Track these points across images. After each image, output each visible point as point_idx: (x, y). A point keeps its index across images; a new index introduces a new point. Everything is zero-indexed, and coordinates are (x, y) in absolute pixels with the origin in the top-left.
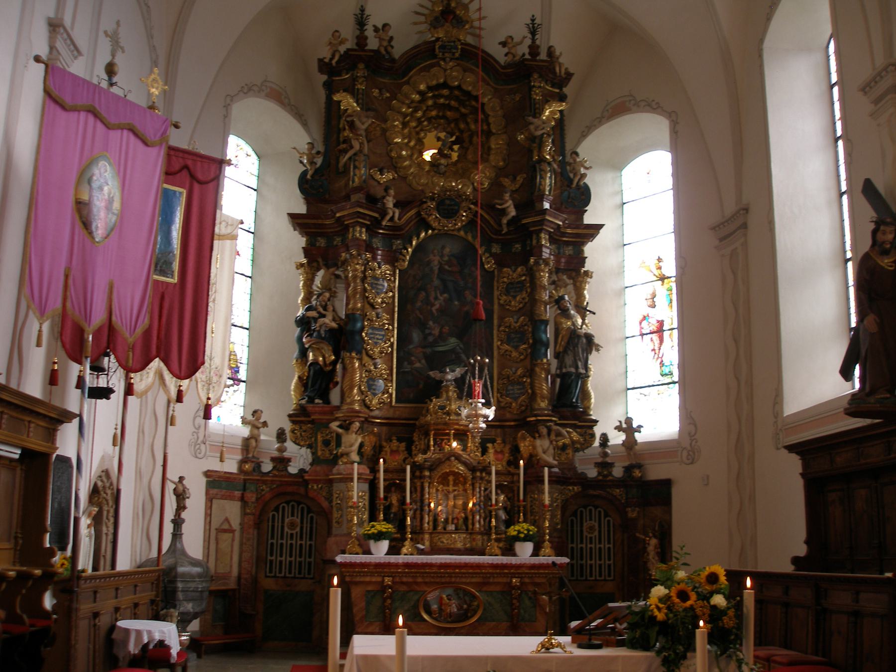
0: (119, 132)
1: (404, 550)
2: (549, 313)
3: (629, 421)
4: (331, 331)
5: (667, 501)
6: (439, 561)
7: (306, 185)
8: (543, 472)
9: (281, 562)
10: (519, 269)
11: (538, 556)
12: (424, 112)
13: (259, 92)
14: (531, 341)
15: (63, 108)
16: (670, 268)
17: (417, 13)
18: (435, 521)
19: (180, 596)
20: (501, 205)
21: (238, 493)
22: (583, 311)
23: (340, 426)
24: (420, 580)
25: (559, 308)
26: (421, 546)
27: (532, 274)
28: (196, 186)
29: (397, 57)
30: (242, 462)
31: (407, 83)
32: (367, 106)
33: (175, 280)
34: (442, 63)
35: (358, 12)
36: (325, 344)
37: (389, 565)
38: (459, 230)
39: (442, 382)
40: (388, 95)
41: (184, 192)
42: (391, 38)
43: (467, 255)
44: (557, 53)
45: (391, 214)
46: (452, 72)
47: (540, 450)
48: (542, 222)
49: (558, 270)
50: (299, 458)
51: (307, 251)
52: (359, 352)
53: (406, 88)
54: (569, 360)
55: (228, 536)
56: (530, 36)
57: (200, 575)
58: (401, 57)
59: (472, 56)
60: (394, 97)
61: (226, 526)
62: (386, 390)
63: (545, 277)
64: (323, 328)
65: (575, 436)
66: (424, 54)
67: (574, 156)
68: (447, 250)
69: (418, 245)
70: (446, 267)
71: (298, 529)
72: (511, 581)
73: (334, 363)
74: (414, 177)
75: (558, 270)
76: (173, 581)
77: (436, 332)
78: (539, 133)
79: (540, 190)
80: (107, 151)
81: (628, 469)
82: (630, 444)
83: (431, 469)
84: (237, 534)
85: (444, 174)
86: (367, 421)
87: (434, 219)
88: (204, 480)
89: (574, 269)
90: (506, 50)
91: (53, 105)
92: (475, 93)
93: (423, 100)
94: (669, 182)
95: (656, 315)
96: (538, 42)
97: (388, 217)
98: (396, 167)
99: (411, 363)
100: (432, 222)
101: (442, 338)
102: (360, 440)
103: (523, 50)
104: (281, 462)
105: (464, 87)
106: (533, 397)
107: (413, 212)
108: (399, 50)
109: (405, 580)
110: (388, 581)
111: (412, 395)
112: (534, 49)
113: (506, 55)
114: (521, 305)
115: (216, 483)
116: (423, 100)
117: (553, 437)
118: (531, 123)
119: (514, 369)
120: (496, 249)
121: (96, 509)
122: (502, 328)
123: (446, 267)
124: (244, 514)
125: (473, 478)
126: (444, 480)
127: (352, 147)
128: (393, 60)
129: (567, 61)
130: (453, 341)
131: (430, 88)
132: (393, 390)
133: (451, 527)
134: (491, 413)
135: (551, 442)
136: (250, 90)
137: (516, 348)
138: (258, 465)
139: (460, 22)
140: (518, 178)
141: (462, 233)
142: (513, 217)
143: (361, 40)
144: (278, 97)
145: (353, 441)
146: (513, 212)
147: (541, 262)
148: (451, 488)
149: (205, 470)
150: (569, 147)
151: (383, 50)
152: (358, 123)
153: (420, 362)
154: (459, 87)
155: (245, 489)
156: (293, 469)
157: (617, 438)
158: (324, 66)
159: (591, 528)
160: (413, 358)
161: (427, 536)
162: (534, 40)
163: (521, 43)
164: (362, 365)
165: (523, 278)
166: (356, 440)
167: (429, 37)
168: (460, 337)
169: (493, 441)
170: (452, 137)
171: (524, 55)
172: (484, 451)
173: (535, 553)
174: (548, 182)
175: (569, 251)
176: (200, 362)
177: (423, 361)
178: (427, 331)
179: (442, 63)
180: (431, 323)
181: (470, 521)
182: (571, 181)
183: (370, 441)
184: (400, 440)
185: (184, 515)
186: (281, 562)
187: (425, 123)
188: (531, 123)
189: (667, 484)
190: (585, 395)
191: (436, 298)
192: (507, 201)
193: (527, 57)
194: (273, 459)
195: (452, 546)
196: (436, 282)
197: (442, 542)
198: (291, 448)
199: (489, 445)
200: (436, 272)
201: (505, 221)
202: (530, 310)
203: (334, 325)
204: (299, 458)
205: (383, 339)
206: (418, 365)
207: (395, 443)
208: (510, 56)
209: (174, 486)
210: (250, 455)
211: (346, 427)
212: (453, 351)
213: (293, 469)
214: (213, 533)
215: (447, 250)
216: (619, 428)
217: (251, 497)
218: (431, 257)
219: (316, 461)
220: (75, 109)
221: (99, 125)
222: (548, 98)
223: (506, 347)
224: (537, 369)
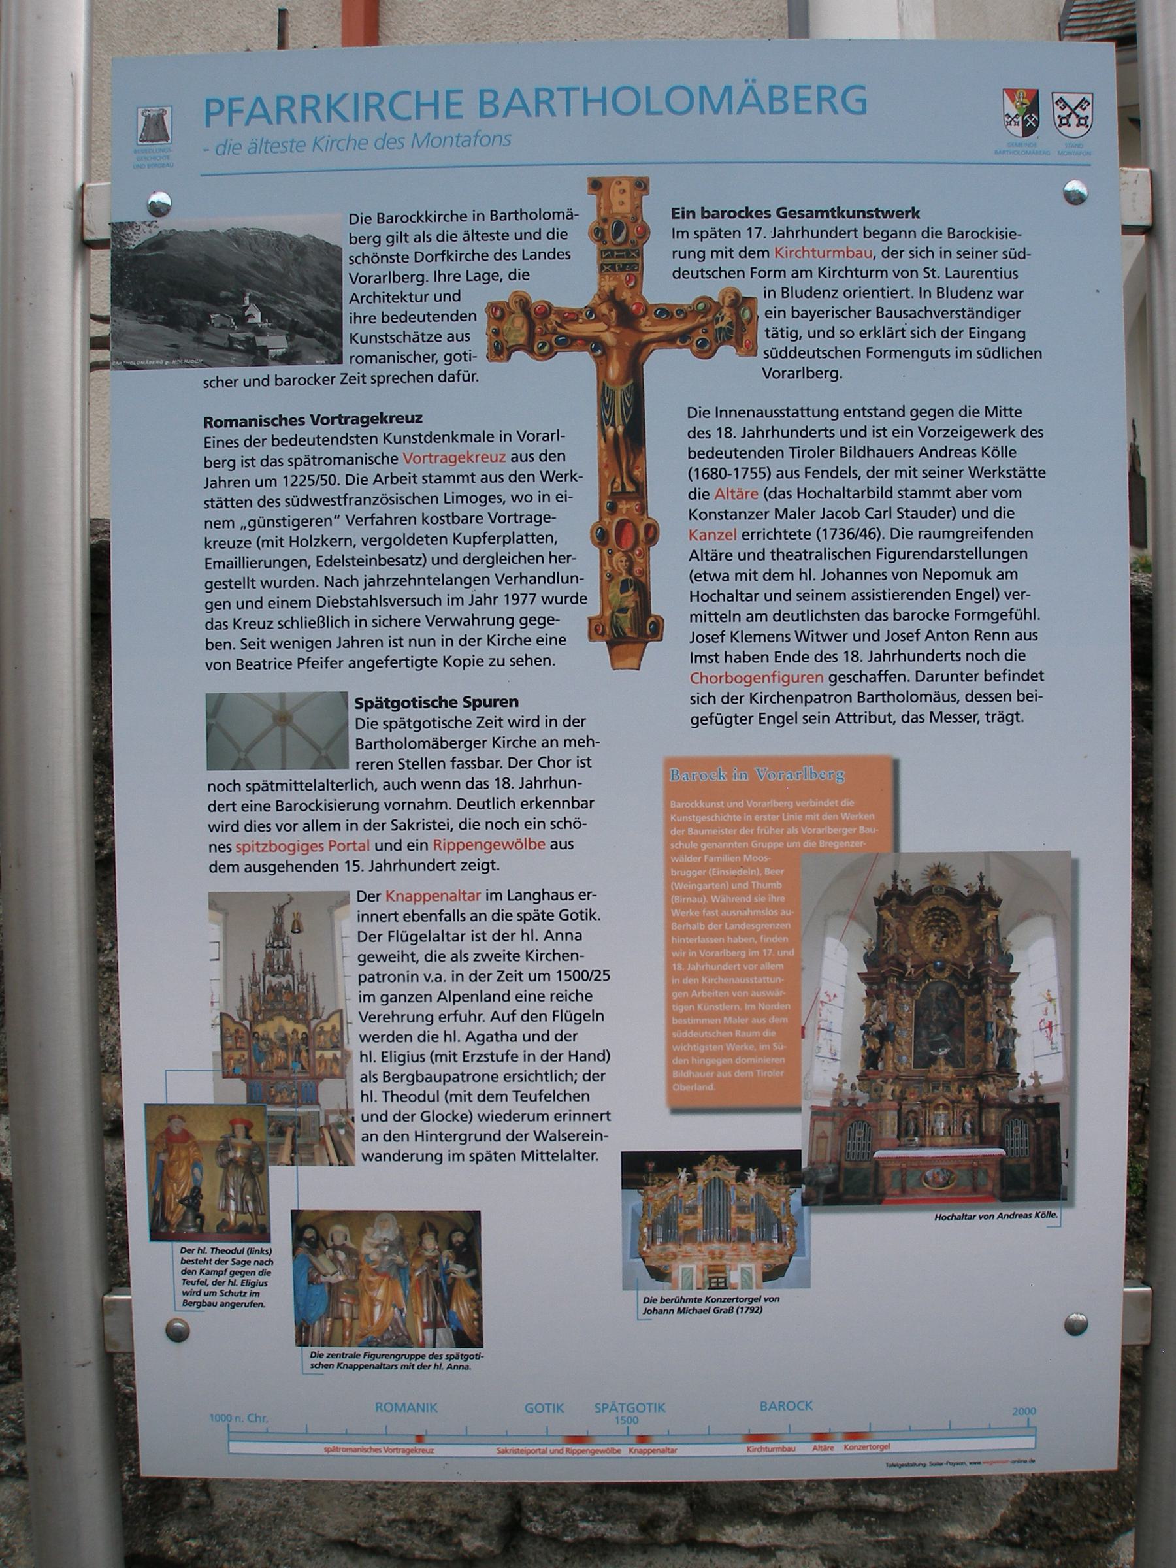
2: (993, 1018)
3: (1036, 1073)
5: (1057, 1114)
7: (867, 959)
16: (1055, 994)
22: (1011, 1016)
27: (983, 998)
32: (896, 916)
36: (877, 1040)
43: (951, 992)
46: (940, 901)
48: (987, 972)
49: (997, 997)
52: (893, 1042)
54: (1004, 1042)
55: (824, 1141)
59: (953, 893)
62: (907, 1061)
63: (990, 999)
65: (1008, 1082)
66: (926, 893)
73: (880, 1048)
75: (997, 997)
81: (1036, 1098)
82: (1037, 1085)
83: (930, 1102)
86: (897, 1078)
89: (1006, 996)
94: (1054, 951)
95: (1048, 1019)
101: (938, 1034)
104: (853, 1101)
108: (914, 892)
112: (982, 888)
120: (965, 987)
121: (992, 1132)
129: (999, 892)
131: (930, 910)
138: (841, 1104)
143: (895, 887)
145: (888, 1089)
150: (1002, 934)
157: (1030, 1083)
158: (877, 901)
159: (1017, 1130)
164: (895, 1049)
168: (947, 1032)
172: (960, 1092)
174: (990, 951)
175: (1002, 987)
183: (898, 1089)
189: (1057, 1105)
190: (1014, 1060)
198: (858, 1093)
202: (983, 1019)
204: (863, 1099)
205: (905, 1034)
211: (885, 1081)
212: (943, 1041)
213: (859, 1104)
216: (1031, 1077)
217: (837, 1119)
219: (871, 1099)
222: (989, 910)
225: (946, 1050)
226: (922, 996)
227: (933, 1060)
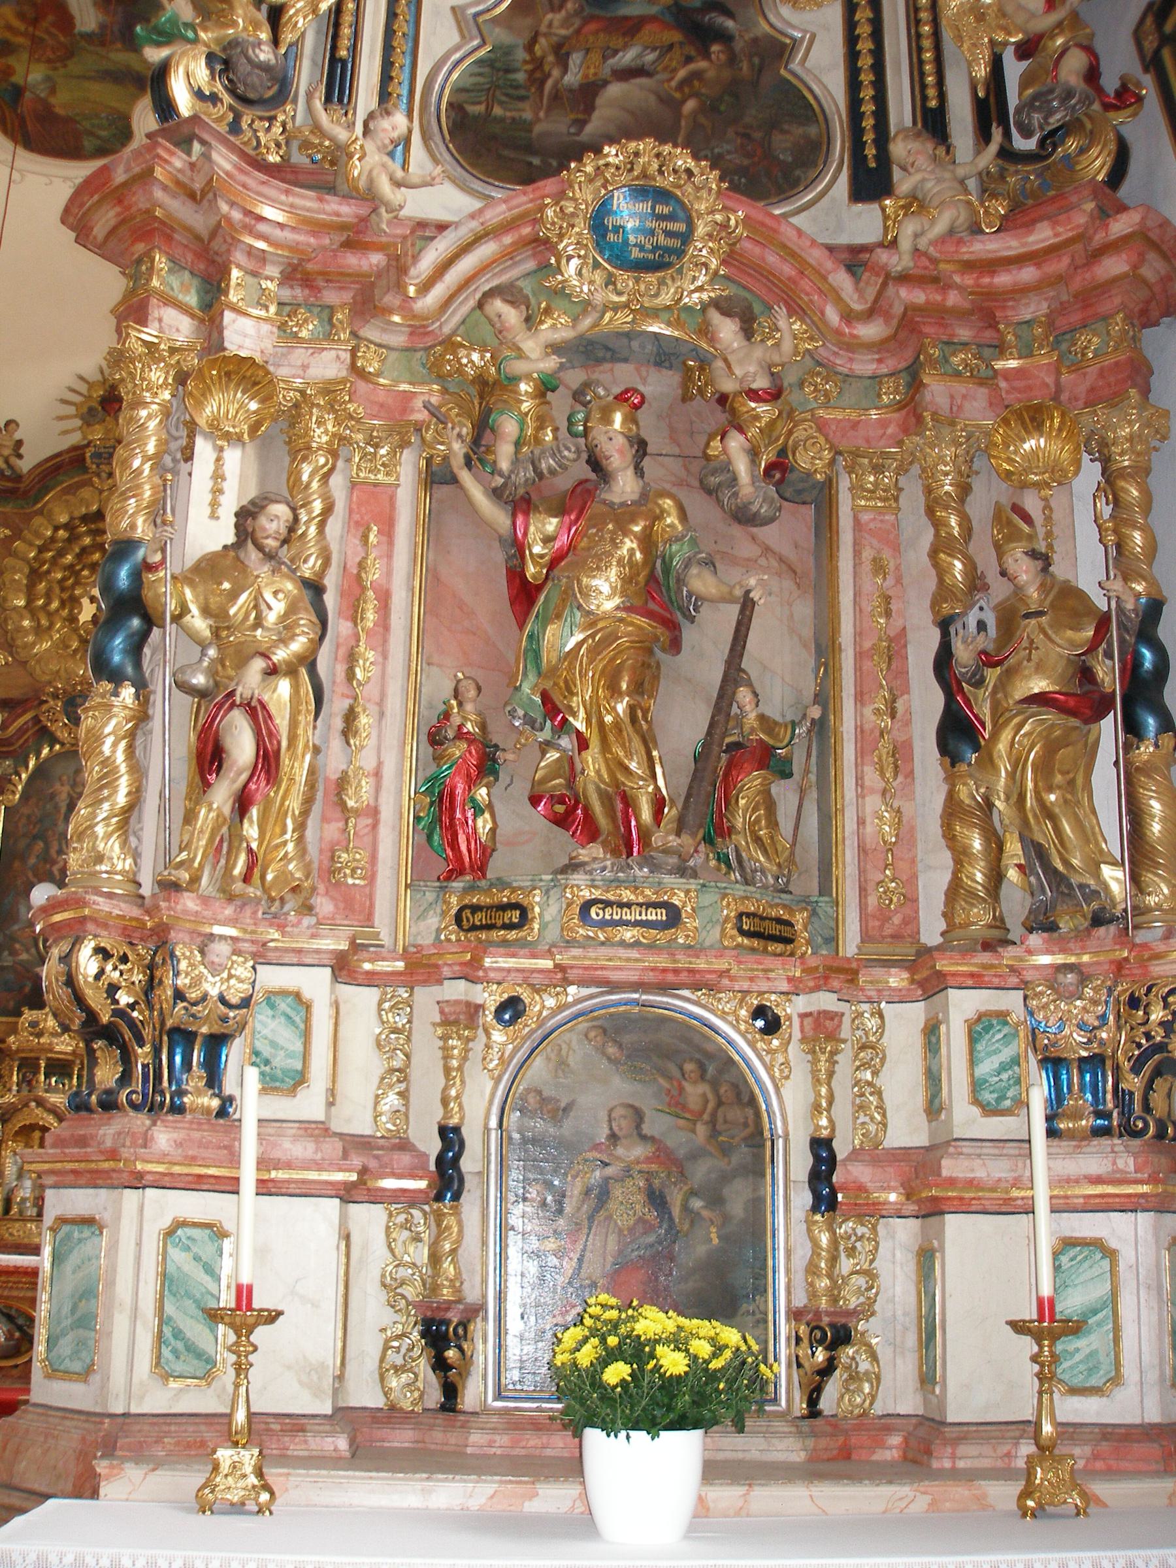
12: (79, 556)
17: (64, 402)
29: (25, 470)
31: (40, 512)
34: (95, 479)
42: (19, 443)
53: (37, 521)
60: (17, 535)
74: (38, 661)
93: (73, 538)
98: (11, 646)
99: (13, 953)
100: (59, 734)
107: (28, 716)
111: (12, 1003)
116: (73, 538)
128: (18, 478)
153: (27, 951)
160: (17, 946)
167: (75, 438)
179: (95, 479)
195: (26, 1241)
197: (11, 1234)
206: (24, 956)
218: (58, 786)
226: (25, 796)
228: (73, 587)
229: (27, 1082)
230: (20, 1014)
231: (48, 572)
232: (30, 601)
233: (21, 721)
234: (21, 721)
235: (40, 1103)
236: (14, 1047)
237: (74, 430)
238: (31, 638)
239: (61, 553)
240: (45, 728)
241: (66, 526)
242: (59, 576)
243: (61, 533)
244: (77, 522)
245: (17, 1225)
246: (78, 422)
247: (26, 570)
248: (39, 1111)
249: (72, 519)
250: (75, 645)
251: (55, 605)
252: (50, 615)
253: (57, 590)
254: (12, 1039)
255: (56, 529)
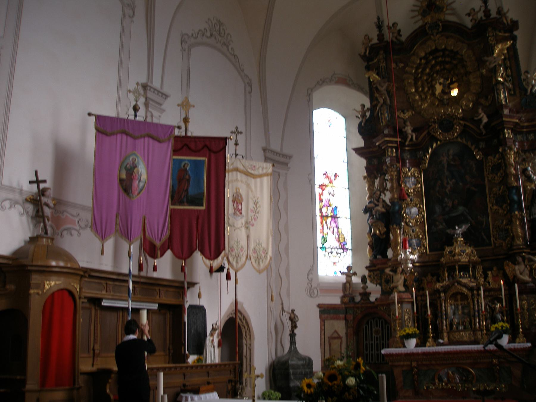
0: (142, 140)
1: (428, 344)
4: (383, 213)
6: (443, 350)
8: (426, 293)
9: (372, 355)
10: (497, 156)
11: (514, 342)
13: (330, 81)
14: (508, 201)
15: (106, 135)
18: (451, 325)
19: (292, 377)
20: (477, 117)
21: (342, 316)
23: (392, 271)
24: (433, 362)
25: (526, 176)
26: (441, 341)
27: (504, 157)
28: (213, 155)
30: (343, 298)
33: (204, 208)
34: (432, 37)
35: (376, 20)
37: (418, 354)
38: (457, 137)
39: (454, 235)
40: (402, 65)
41: (205, 159)
42: (399, 31)
44: (505, 10)
45: (410, 137)
47: (518, 273)
50: (375, 291)
51: (367, 169)
55: (338, 341)
56: (483, 5)
57: (303, 365)
58: (406, 40)
61: (335, 335)
64: (378, 213)
66: (420, 34)
67: (526, 74)
68: (451, 152)
69: (432, 153)
70: (452, 163)
71: (381, 334)
72: (492, 361)
76: (287, 369)
77: (450, 204)
78: (492, 66)
79: (499, 102)
80: (135, 150)
84: (344, 340)
85: (448, 104)
87: (439, 134)
88: (318, 310)
90: (471, 18)
91: (100, 135)
92: (455, 50)
96: (489, 7)
97: (408, 140)
100: (438, 137)
102: (403, 278)
103: (481, 15)
104: (366, 295)
105: (449, 48)
106: (513, 238)
107: (425, 133)
109: (424, 363)
110: (414, 364)
113: (471, 21)
114: (501, 179)
115: (326, 312)
116: (427, 63)
117: (526, 262)
118: (487, 61)
119: (501, 221)
122: (492, 195)
123: (452, 163)
124: (347, 327)
125: (473, 295)
126: (454, 296)
127: (379, 102)
128: (402, 43)
130: (461, 208)
132: (426, 245)
133: (461, 328)
134: (414, 257)
135: (526, 266)
136: (323, 82)
137: (501, 207)
138: (353, 299)
139: (440, 9)
140: (489, 97)
141: (459, 140)
142: (486, 123)
144: (344, 81)
146: (485, 120)
147: (507, 149)
148: (459, 303)
149: (317, 303)
151: (394, 39)
152: (379, 87)
154: (445, 49)
155: (346, 313)
156: (372, 299)
158: (364, 57)
160: (437, 223)
161: (445, 334)
162: (486, 7)
163: (480, 10)
165: (500, 161)
166: (401, 278)
167: (420, 23)
169: (491, 269)
170: (448, 80)
171: (481, 18)
173: (417, 345)
176: (222, 248)
177: (444, 224)
178: (444, 205)
179: (432, 37)
180: (446, 199)
181: (473, 323)
182: (526, 90)
184: (433, 275)
185: (296, 331)
186: (372, 355)
187: (435, 75)
188: (487, 61)
191: (448, 183)
192: (480, 114)
193: (484, 18)
194: (361, 294)
195: (461, 340)
196: (447, 173)
197: (455, 338)
198: (371, 286)
199: (489, 273)
200: (446, 166)
201: (481, 127)
203: (383, 210)
206: (441, 227)
207: (429, 277)
208: (473, 21)
209: (289, 315)
210: (348, 292)
213: (372, 299)
214: (327, 340)
215: (451, 152)
217: (350, 317)
220: (112, 134)
221: (129, 138)
223: (495, 207)
224: (514, 220)
225: (464, 228)
227: (450, 241)
228: (431, 81)
229: (452, 275)
230: (444, 249)
231: (421, 77)
232: (416, 90)
233: (423, 135)
234: (423, 135)
235: (459, 283)
236: (444, 262)
237: (419, 20)
238: (420, 103)
239: (424, 69)
240: (433, 136)
241: (424, 58)
242: (425, 78)
243: (423, 61)
244: (428, 56)
245: (456, 334)
246: (420, 17)
247: (413, 78)
248: (459, 287)
249: (426, 54)
250: (437, 103)
251: (426, 89)
252: (425, 94)
253: (426, 84)
254: (443, 259)
255: (421, 60)
